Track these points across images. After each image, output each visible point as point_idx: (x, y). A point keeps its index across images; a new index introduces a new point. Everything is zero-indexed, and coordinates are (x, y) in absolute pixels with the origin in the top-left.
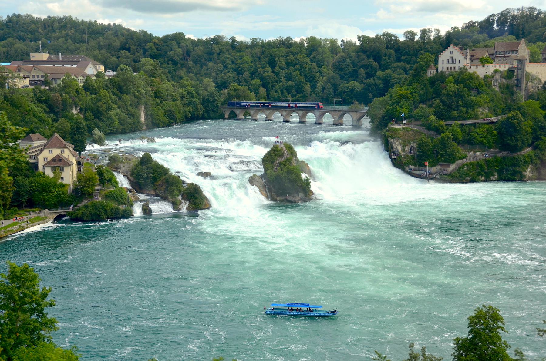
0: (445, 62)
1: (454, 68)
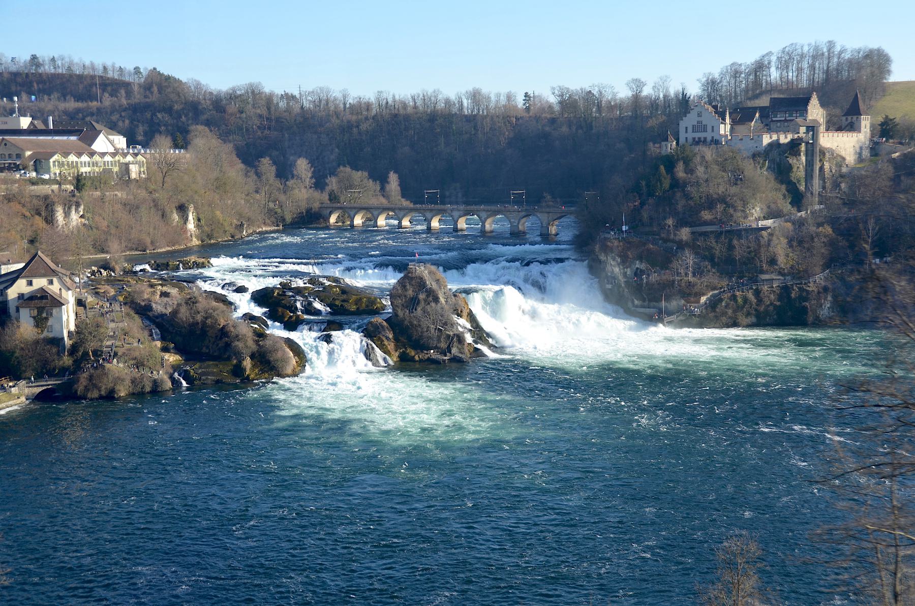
0: (690, 130)
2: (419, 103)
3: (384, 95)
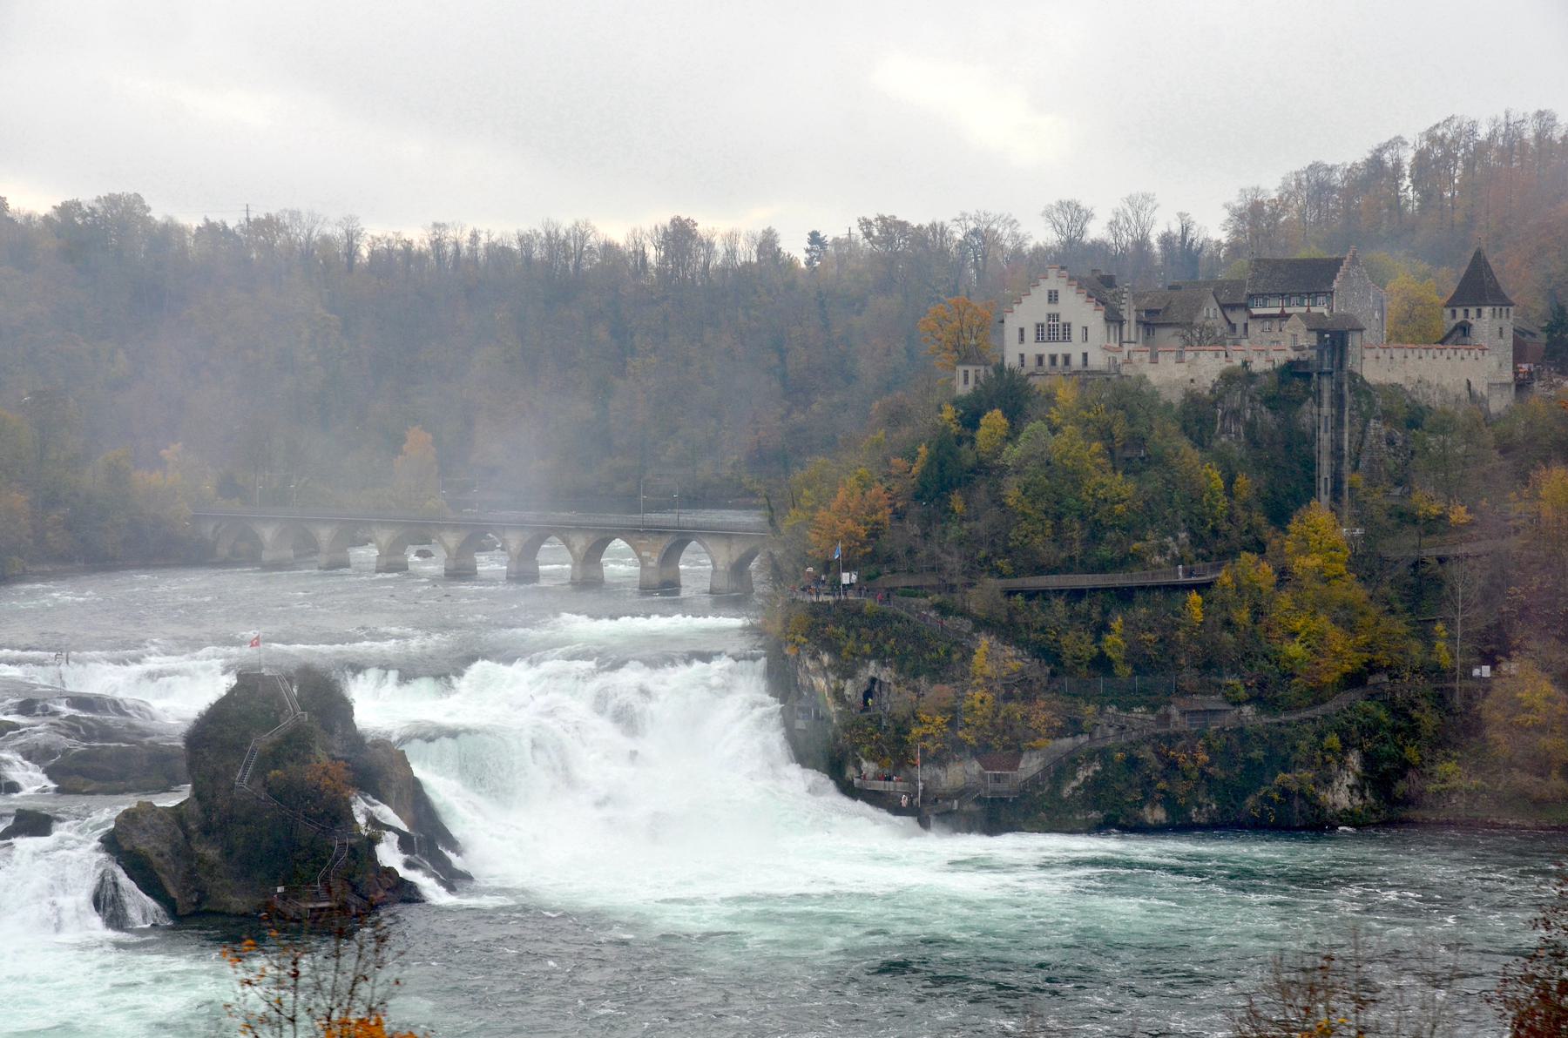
0: (1030, 334)
1: (1067, 359)
2: (538, 253)
3: (451, 234)
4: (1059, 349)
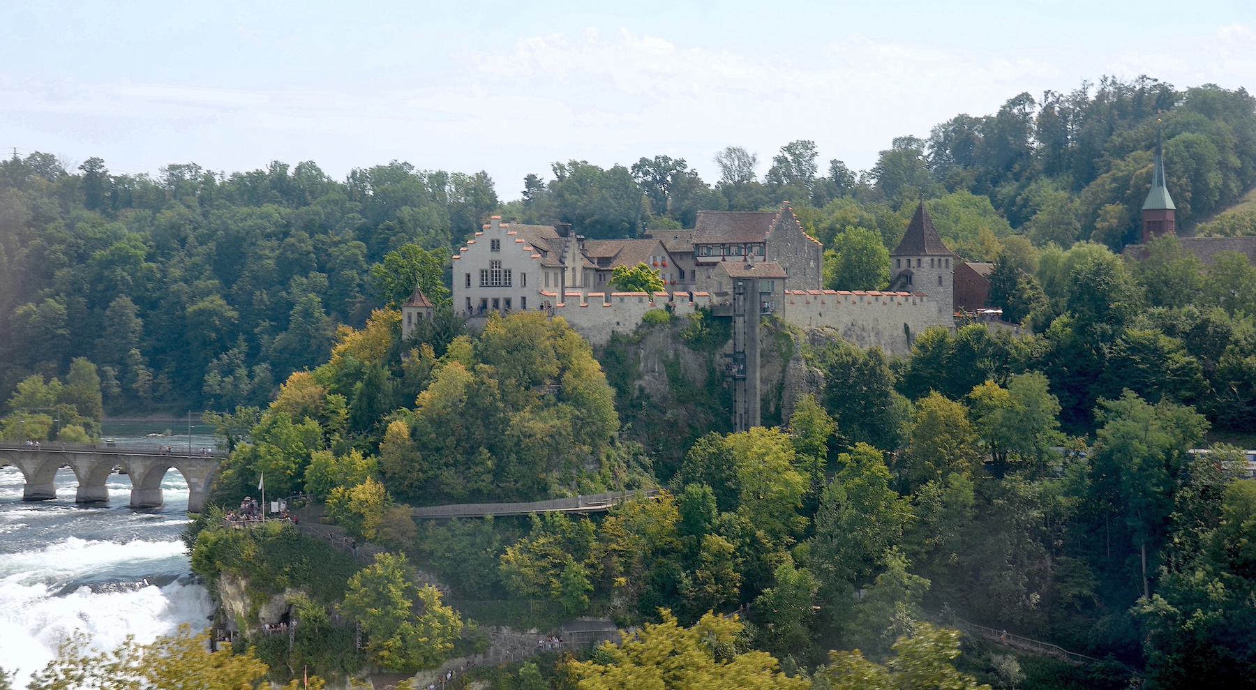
0: (476, 280)
4: (500, 293)
